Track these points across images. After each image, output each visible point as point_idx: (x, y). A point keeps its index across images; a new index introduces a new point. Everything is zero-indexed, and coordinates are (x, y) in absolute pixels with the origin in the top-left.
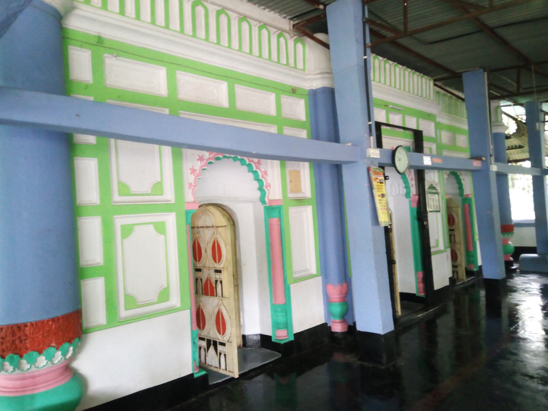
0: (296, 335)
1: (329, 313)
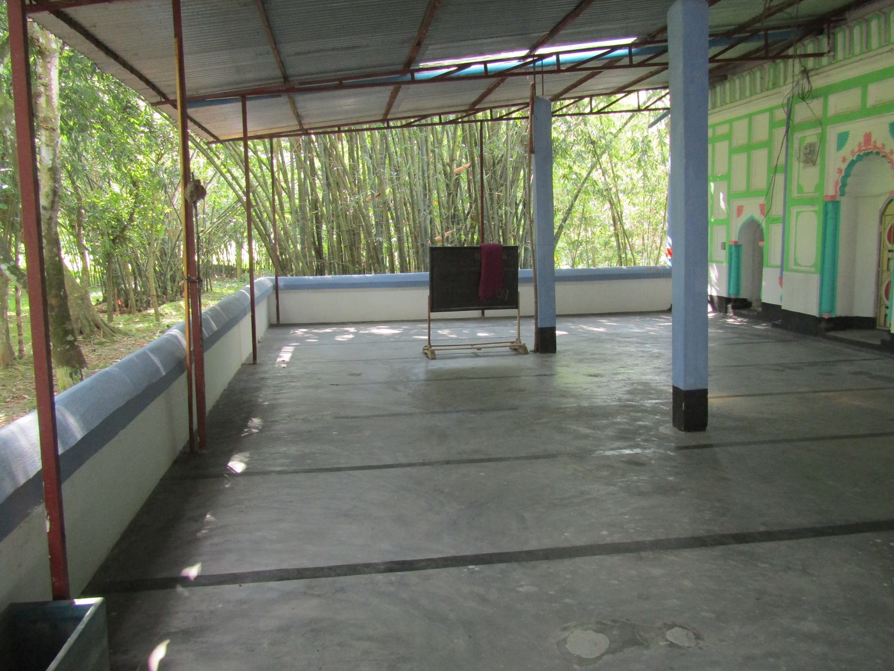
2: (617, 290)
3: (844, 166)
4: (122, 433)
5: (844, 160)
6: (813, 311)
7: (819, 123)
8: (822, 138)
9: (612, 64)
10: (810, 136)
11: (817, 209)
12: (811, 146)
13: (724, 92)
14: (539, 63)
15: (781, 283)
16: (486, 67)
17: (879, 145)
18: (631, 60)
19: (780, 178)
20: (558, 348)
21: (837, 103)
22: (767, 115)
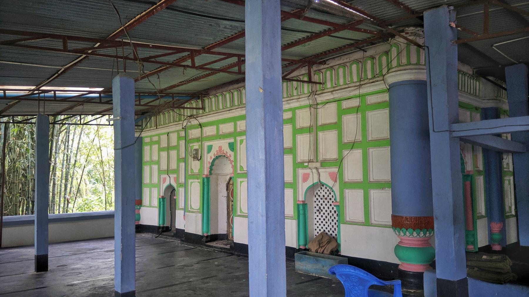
0: (479, 248)
1: (491, 239)
2: (89, 228)
3: (211, 161)
4: (119, 97)
5: (211, 157)
6: (200, 233)
7: (200, 139)
8: (202, 146)
9: (90, 100)
10: (196, 146)
11: (199, 181)
12: (197, 150)
13: (165, 117)
14: (42, 95)
15: (184, 219)
16: (5, 93)
17: (225, 152)
18: (100, 100)
19: (182, 165)
20: (49, 269)
21: (209, 131)
22: (176, 134)
